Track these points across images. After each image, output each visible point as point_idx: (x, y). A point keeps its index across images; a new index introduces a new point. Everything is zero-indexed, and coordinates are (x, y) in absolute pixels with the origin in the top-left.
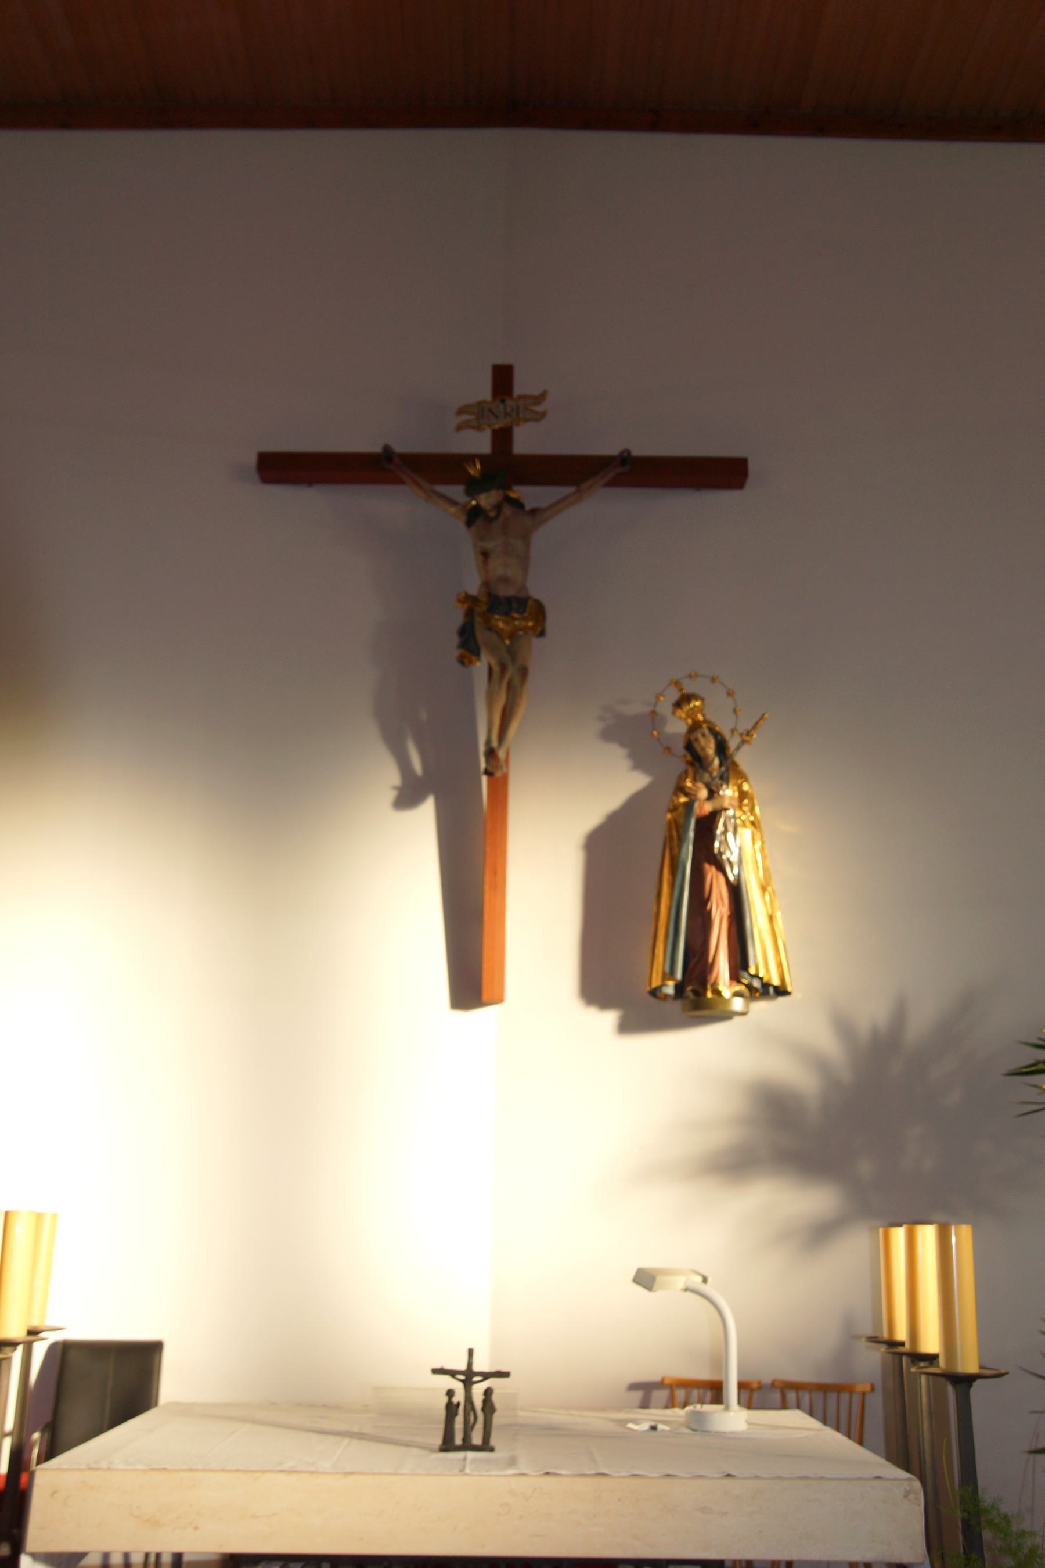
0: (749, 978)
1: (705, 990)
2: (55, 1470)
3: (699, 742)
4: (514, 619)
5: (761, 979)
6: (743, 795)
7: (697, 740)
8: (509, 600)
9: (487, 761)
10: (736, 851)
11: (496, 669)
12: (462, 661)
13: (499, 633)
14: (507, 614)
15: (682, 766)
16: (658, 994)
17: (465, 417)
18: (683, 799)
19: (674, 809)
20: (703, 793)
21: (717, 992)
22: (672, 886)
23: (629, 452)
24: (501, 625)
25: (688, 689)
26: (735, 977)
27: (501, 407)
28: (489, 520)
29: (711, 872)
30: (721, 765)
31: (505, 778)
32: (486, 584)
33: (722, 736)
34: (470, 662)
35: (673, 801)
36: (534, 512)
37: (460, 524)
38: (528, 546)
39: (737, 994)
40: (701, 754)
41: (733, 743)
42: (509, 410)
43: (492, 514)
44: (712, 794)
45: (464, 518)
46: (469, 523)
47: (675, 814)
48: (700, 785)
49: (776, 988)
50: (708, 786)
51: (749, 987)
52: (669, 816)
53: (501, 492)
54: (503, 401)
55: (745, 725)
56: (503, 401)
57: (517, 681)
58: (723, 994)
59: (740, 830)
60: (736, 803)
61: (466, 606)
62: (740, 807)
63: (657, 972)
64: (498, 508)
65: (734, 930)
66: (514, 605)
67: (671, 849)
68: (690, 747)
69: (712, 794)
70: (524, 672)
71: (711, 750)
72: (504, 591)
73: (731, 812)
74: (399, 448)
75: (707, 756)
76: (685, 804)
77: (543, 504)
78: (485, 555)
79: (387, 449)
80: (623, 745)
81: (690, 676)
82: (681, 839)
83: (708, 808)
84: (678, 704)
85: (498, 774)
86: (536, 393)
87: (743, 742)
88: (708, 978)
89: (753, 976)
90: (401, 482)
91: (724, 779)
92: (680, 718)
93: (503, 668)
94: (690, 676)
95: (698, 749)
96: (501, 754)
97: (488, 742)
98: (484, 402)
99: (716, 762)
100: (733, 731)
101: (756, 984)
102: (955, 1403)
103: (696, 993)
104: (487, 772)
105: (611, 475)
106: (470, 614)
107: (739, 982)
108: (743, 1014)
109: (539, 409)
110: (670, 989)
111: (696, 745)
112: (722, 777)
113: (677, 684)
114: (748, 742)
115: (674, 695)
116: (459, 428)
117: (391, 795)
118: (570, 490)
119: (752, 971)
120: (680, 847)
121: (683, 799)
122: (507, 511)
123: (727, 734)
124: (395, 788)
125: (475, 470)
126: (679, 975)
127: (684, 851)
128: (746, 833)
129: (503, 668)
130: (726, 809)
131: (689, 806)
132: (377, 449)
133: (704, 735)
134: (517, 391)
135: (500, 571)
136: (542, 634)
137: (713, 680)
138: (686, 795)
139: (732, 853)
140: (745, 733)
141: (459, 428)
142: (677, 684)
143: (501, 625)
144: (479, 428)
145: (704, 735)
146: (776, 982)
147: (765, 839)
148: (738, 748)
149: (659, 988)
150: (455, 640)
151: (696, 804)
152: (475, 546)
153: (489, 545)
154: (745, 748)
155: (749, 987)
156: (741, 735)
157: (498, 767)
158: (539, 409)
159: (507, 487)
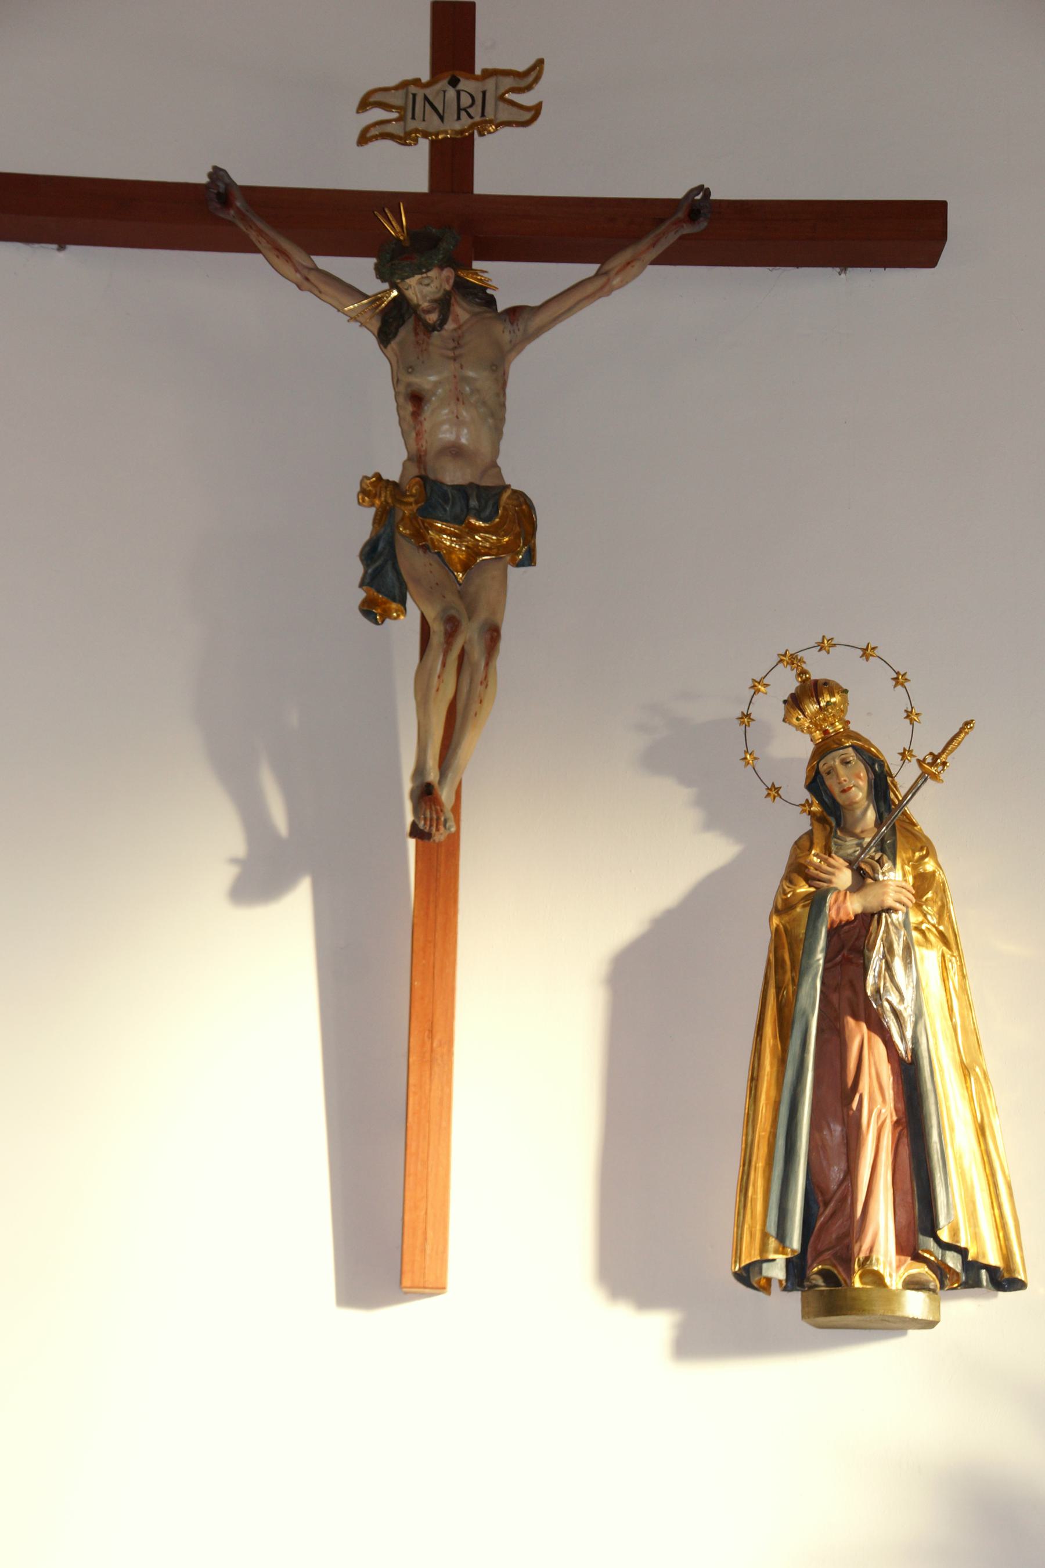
0: (938, 1252)
1: (850, 1273)
2: (424, 107)
4: (477, 530)
6: (923, 883)
8: (463, 491)
9: (416, 811)
10: (909, 994)
11: (437, 629)
12: (370, 610)
13: (442, 557)
14: (459, 519)
15: (804, 823)
16: (754, 1280)
17: (377, 114)
18: (804, 889)
19: (398, 616)
20: (844, 878)
21: (878, 1279)
23: (707, 192)
24: (447, 540)
25: (816, 674)
26: (908, 1248)
27: (451, 93)
28: (430, 329)
29: (858, 1033)
30: (880, 822)
31: (453, 842)
32: (417, 458)
33: (882, 764)
34: (386, 615)
35: (785, 893)
36: (514, 312)
37: (369, 340)
38: (502, 384)
39: (914, 1284)
40: (840, 799)
41: (904, 777)
42: (465, 101)
43: (433, 318)
44: (862, 878)
45: (376, 324)
46: (384, 337)
47: (786, 918)
48: (838, 861)
49: (992, 1270)
50: (853, 864)
51: (940, 1270)
52: (776, 921)
53: (448, 272)
54: (454, 82)
55: (927, 743)
56: (454, 82)
57: (477, 653)
58: (887, 1281)
59: (920, 952)
60: (908, 898)
62: (918, 906)
63: (752, 1235)
64: (444, 304)
65: (905, 1152)
66: (474, 503)
67: (779, 989)
68: (816, 783)
69: (862, 878)
70: (493, 635)
71: (859, 792)
72: (453, 475)
73: (897, 917)
74: (242, 176)
75: (852, 804)
76: (808, 896)
77: (534, 300)
78: (416, 400)
79: (218, 174)
80: (685, 780)
81: (821, 646)
82: (800, 969)
83: (854, 905)
84: (795, 702)
85: (440, 836)
86: (521, 65)
87: (925, 776)
88: (856, 1248)
90: (247, 247)
91: (887, 848)
92: (799, 728)
93: (452, 626)
94: (821, 646)
95: (836, 791)
96: (446, 796)
97: (419, 771)
98: (417, 82)
99: (871, 815)
101: (953, 1261)
103: (829, 1277)
104: (416, 832)
105: (671, 238)
106: (384, 518)
107: (917, 1258)
108: (930, 1324)
109: (526, 99)
110: (777, 1271)
111: (830, 782)
113: (792, 660)
114: (935, 777)
115: (787, 683)
116: (364, 139)
117: (228, 874)
118: (589, 269)
119: (944, 1235)
120: (797, 984)
121: (804, 889)
122: (461, 312)
123: (892, 761)
124: (234, 861)
125: (395, 228)
126: (795, 1242)
128: (928, 958)
129: (452, 626)
130: (889, 910)
131: (817, 902)
132: (200, 177)
133: (845, 763)
134: (482, 63)
135: (447, 434)
136: (530, 559)
137: (867, 652)
138: (809, 879)
139: (902, 999)
140: (929, 759)
141: (364, 139)
142: (792, 660)
143: (447, 540)
144: (405, 139)
145: (845, 763)
146: (994, 1259)
148: (914, 789)
150: (358, 570)
151: (830, 899)
152: (396, 382)
153: (427, 380)
155: (940, 1270)
156: (920, 763)
157: (438, 822)
158: (526, 99)
159: (459, 262)
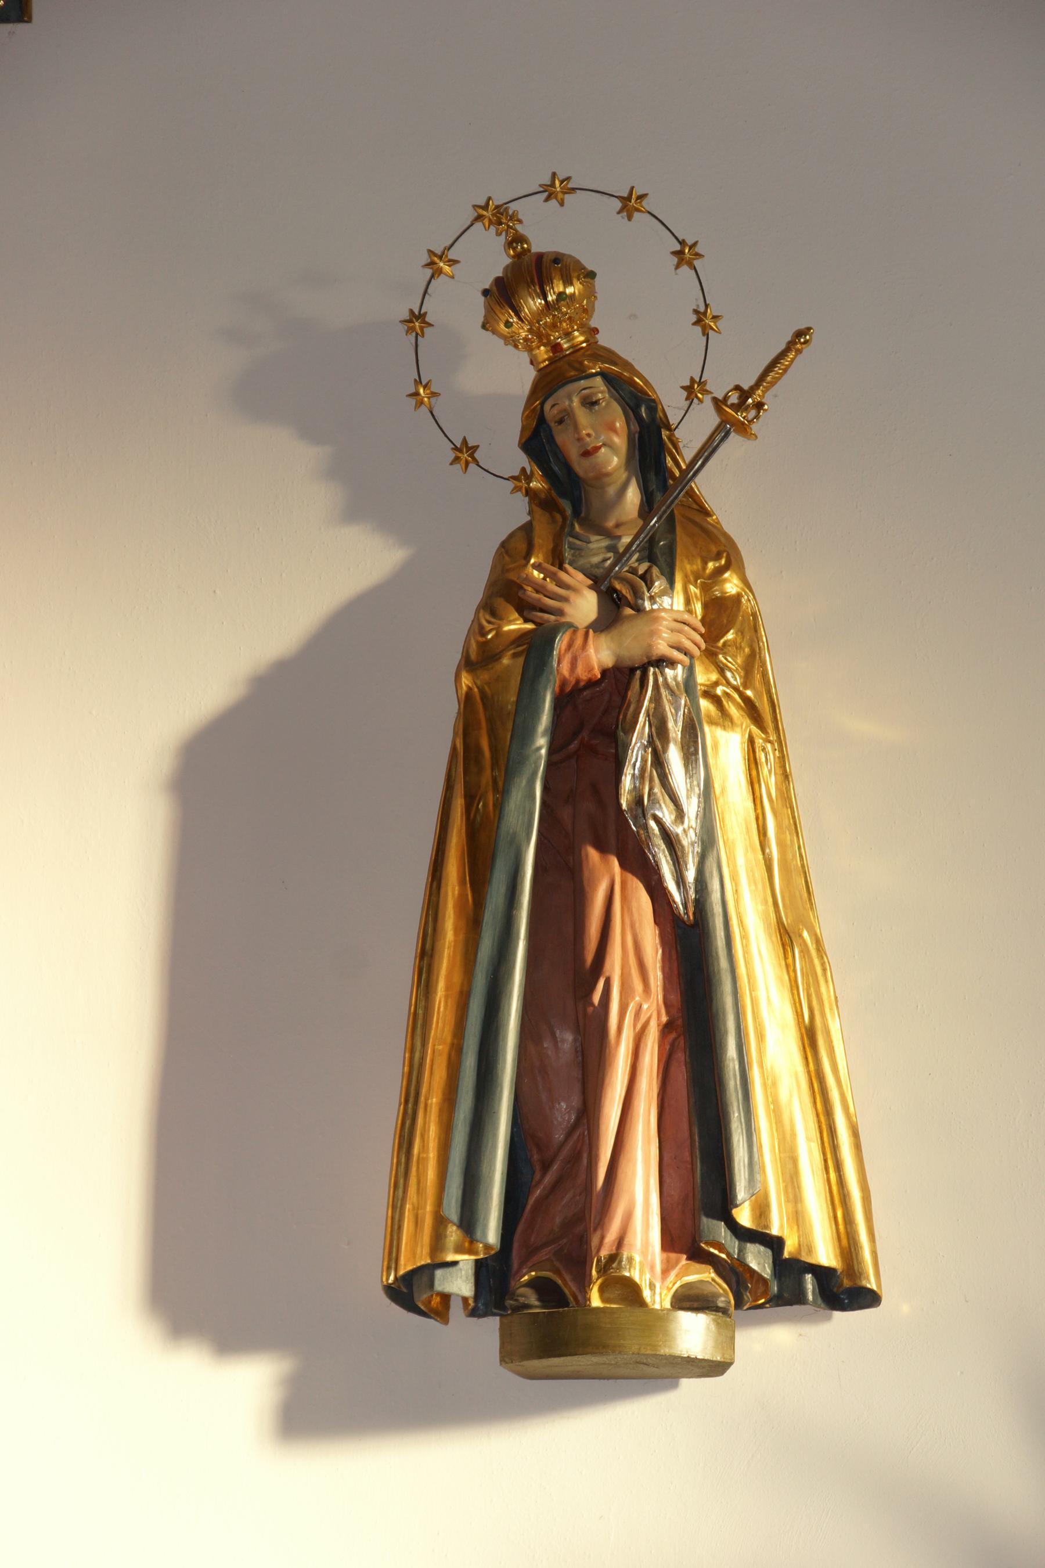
1: (584, 1283)
3: (576, 427)
5: (775, 1244)
7: (566, 418)
18: (515, 625)
21: (631, 1293)
22: (473, 923)
30: (647, 508)
33: (653, 405)
40: (580, 467)
47: (485, 676)
48: (576, 578)
49: (822, 1274)
50: (600, 582)
60: (693, 640)
61: (495, 1247)
62: (711, 654)
63: (417, 1222)
65: (680, 1075)
73: (675, 675)
75: (601, 477)
76: (522, 637)
81: (549, 192)
88: (595, 1241)
89: (744, 1235)
92: (511, 340)
94: (549, 192)
99: (633, 496)
100: (693, 390)
101: (758, 1260)
102: (460, 1193)
103: (546, 1290)
107: (698, 1256)
108: (715, 1368)
111: (563, 438)
112: (650, 555)
119: (744, 1216)
120: (502, 792)
121: (515, 625)
126: (492, 1233)
127: (516, 797)
130: (662, 662)
133: (590, 403)
138: (525, 609)
145: (590, 403)
146: (826, 1255)
147: (794, 766)
148: (707, 451)
149: (424, 1274)
151: (561, 642)
154: (734, 445)
156: (719, 404)
